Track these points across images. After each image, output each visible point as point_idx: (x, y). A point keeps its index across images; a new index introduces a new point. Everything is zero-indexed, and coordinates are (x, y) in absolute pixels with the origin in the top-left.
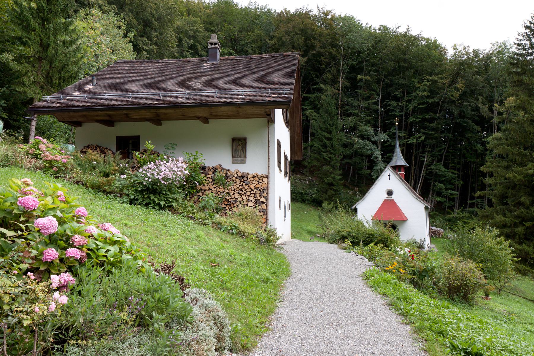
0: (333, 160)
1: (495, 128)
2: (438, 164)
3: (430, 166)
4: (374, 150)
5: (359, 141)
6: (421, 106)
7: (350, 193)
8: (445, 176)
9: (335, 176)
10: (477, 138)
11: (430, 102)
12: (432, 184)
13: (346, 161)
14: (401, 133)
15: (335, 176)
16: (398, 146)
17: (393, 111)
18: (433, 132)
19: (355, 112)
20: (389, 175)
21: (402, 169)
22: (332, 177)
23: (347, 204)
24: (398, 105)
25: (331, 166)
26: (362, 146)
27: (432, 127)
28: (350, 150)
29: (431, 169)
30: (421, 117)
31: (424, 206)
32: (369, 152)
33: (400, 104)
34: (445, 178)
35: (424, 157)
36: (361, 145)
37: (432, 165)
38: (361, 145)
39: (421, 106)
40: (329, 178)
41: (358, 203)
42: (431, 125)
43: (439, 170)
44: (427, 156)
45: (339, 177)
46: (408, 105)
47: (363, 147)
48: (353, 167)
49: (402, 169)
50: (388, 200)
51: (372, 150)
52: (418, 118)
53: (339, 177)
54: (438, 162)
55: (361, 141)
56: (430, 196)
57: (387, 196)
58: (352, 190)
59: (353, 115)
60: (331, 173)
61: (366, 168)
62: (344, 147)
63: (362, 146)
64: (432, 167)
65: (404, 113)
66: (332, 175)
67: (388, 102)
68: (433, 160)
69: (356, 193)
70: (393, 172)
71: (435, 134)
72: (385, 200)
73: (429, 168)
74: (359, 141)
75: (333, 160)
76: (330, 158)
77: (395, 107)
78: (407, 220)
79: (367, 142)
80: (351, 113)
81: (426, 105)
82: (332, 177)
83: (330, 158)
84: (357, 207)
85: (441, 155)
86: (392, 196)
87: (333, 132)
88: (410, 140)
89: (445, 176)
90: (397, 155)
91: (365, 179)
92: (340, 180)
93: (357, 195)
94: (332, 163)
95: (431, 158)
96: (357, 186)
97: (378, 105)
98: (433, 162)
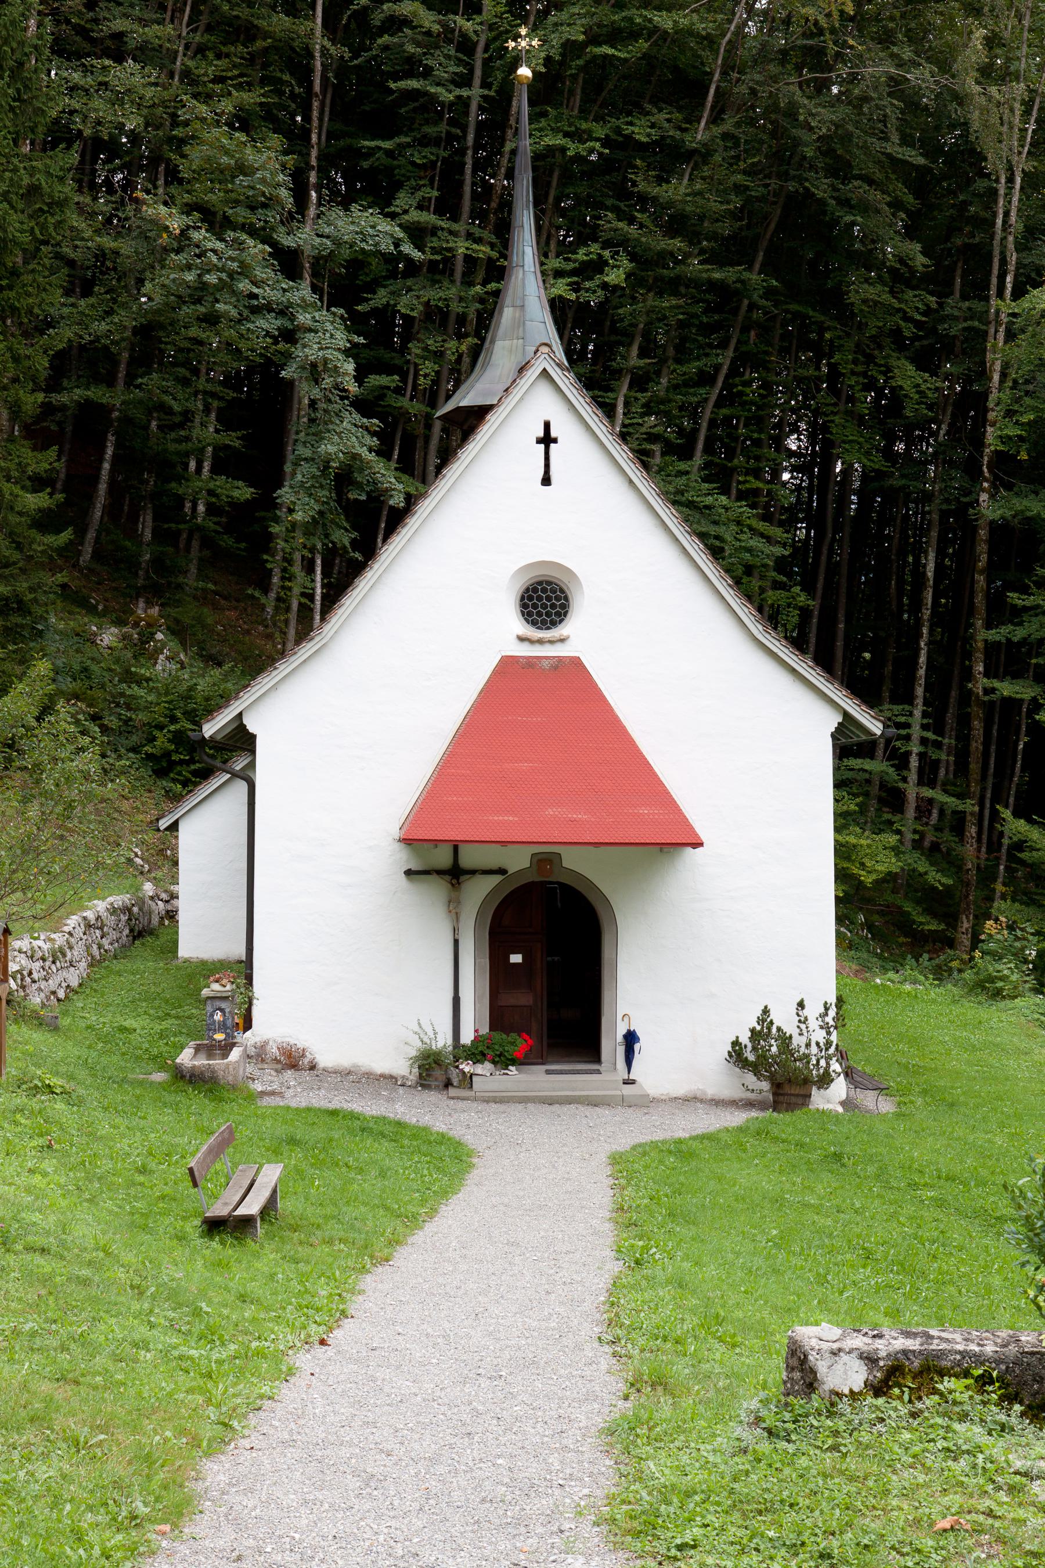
1: (1003, 262)
4: (304, 318)
5: (196, 236)
7: (109, 637)
10: (906, 318)
13: (78, 394)
17: (411, 67)
19: (153, 31)
20: (547, 440)
23: (95, 718)
28: (109, 313)
30: (600, 131)
31: (833, 720)
41: (265, 682)
45: (35, 501)
47: (222, 286)
48: (118, 446)
50: (531, 663)
51: (284, 311)
53: (35, 501)
57: (520, 627)
61: (207, 466)
63: (211, 279)
69: (147, 637)
72: (507, 666)
74: (196, 236)
79: (256, 249)
80: (119, 36)
81: (643, 45)
84: (252, 725)
90: (520, 323)
91: (195, 544)
93: (158, 651)
96: (154, 592)
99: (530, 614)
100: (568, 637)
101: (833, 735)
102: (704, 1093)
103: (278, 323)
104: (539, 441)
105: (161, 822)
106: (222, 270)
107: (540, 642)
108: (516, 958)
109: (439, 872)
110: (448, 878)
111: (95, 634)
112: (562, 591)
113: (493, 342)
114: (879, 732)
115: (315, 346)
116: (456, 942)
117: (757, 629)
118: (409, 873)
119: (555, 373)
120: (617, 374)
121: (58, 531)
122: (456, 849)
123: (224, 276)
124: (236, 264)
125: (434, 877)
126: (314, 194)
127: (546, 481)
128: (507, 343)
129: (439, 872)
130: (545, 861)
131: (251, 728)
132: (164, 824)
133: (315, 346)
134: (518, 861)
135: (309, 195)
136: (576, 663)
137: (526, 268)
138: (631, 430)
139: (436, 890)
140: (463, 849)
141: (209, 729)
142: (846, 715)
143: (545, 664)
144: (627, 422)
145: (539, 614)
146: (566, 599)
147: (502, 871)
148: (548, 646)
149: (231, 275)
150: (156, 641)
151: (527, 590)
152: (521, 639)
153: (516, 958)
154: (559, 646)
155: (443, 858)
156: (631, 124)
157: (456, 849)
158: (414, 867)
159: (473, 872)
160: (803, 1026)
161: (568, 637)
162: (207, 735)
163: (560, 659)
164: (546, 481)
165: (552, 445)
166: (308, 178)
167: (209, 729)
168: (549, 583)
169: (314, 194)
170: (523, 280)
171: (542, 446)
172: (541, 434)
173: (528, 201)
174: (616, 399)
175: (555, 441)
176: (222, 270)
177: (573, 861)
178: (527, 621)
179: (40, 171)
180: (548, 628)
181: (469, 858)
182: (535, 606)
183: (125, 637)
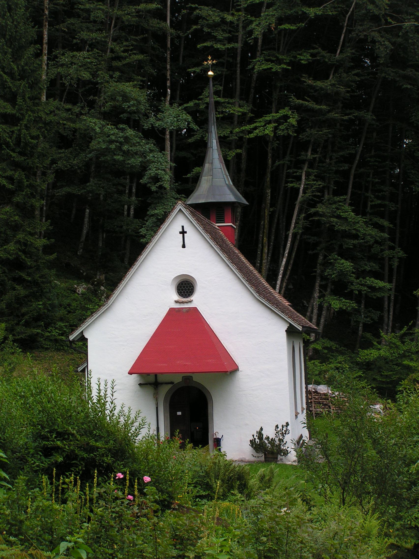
0: (20, 187)
2: (337, 199)
3: (314, 206)
4: (150, 157)
6: (286, 26)
8: (356, 237)
9: (30, 239)
11: (312, 15)
12: (321, 258)
13: (67, 189)
14: (233, 104)
15: (30, 239)
16: (214, 143)
17: (209, 37)
18: (324, 107)
20: (183, 232)
21: (228, 214)
22: (18, 242)
24: (223, 21)
25: (17, 205)
26: (113, 146)
27: (321, 89)
29: (316, 214)
32: (136, 161)
33: (229, 18)
34: (356, 242)
35: (299, 179)
36: (111, 142)
37: (321, 202)
38: (111, 142)
39: (286, 26)
40: (11, 247)
42: (319, 84)
43: (339, 217)
44: (308, 175)
46: (251, 22)
49: (228, 214)
50: (179, 310)
51: (143, 155)
52: (279, 62)
54: (336, 193)
55: (110, 129)
56: (316, 295)
57: (176, 297)
58: (88, 279)
59: (92, 46)
60: (16, 228)
62: (60, 148)
63: (113, 146)
64: (320, 209)
65: (238, 45)
66: (20, 236)
67: (196, 8)
68: (321, 190)
70: (195, 222)
71: (329, 111)
72: (171, 310)
73: (313, 210)
75: (20, 187)
76: (10, 179)
77: (215, 26)
78: (236, 369)
79: (130, 132)
82: (18, 242)
83: (10, 179)
85: (346, 174)
86: (193, 298)
87: (19, 100)
88: (255, 128)
89: (356, 237)
90: (211, 170)
92: (47, 250)
94: (17, 199)
95: (320, 183)
97: (165, 20)
98: (323, 196)
99: (181, 293)
100: (192, 300)
101: (286, 331)
102: (245, 459)
103: (140, 159)
104: (180, 233)
105: (78, 369)
106: (117, 142)
107: (183, 302)
108: (179, 413)
109: (150, 384)
110: (153, 386)
111: (76, 289)
112: (191, 284)
113: (201, 177)
114: (301, 330)
115: (154, 169)
116: (157, 408)
117: (256, 295)
118: (140, 384)
119: (184, 210)
120: (303, 162)
121: (51, 254)
122: (156, 376)
123: (118, 144)
124: (122, 139)
125: (149, 386)
126: (169, 90)
127: (184, 246)
128: (206, 178)
129: (150, 384)
130: (187, 379)
131: (86, 336)
132: (80, 369)
133: (154, 169)
134: (178, 379)
135: (167, 91)
136: (195, 309)
137: (214, 148)
138: (309, 186)
139: (150, 390)
140: (158, 375)
141: (71, 338)
142: (290, 324)
143: (184, 310)
144: (307, 183)
145: (184, 292)
146: (193, 286)
147: (172, 383)
148: (186, 304)
149: (121, 143)
150: (101, 290)
151: (179, 284)
152: (176, 302)
153: (179, 413)
154: (189, 304)
155: (152, 379)
156: (300, 55)
157: (156, 376)
158: (142, 382)
159: (162, 384)
160: (277, 434)
161: (192, 300)
162: (71, 340)
163: (190, 308)
164: (184, 246)
165: (185, 234)
166: (167, 83)
167: (71, 338)
168: (187, 281)
169: (169, 90)
170: (213, 152)
171: (182, 235)
172: (181, 230)
173: (214, 122)
174: (302, 173)
175: (180, 233)
176: (117, 142)
177: (196, 378)
178: (179, 295)
179: (41, 111)
180: (187, 297)
181: (161, 379)
182: (182, 290)
183: (88, 289)
